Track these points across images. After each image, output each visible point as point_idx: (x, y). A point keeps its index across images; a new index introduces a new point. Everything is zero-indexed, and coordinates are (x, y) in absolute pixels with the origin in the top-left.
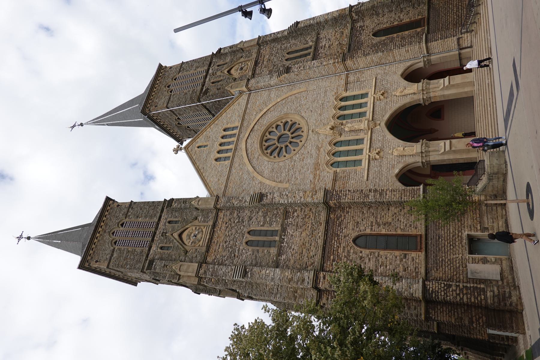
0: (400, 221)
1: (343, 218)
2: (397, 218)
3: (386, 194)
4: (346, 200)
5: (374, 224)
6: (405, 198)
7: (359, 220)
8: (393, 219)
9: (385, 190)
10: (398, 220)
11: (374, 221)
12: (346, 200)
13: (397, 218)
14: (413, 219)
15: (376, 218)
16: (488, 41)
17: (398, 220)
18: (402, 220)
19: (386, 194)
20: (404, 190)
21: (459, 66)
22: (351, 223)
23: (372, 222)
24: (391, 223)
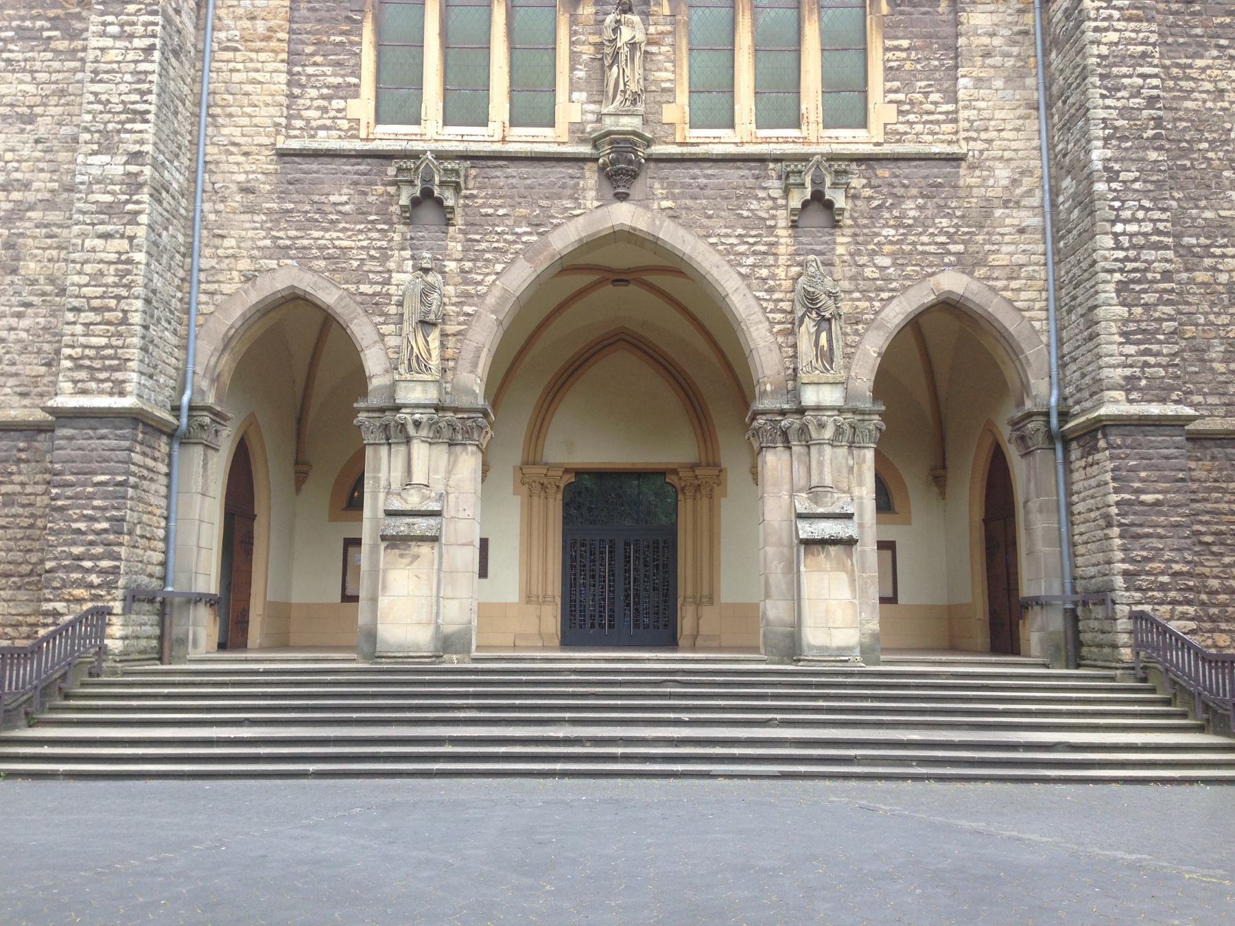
0: (19, 315)
1: (62, 45)
2: (36, 300)
3: (106, 236)
4: (94, 42)
5: (16, 196)
6: (79, 329)
7: (43, 126)
8: (34, 282)
9: (130, 230)
10: (28, 305)
11: (31, 197)
12: (94, 42)
13: (36, 300)
14: (28, 370)
15: (49, 204)
16: (1075, 769)
17: (28, 305)
18: (24, 323)
19: (106, 236)
20: (124, 321)
21: (723, 600)
22: (31, 89)
23: (26, 186)
24: (14, 271)
